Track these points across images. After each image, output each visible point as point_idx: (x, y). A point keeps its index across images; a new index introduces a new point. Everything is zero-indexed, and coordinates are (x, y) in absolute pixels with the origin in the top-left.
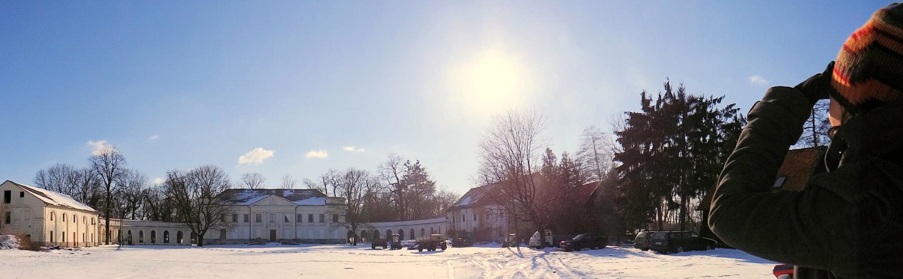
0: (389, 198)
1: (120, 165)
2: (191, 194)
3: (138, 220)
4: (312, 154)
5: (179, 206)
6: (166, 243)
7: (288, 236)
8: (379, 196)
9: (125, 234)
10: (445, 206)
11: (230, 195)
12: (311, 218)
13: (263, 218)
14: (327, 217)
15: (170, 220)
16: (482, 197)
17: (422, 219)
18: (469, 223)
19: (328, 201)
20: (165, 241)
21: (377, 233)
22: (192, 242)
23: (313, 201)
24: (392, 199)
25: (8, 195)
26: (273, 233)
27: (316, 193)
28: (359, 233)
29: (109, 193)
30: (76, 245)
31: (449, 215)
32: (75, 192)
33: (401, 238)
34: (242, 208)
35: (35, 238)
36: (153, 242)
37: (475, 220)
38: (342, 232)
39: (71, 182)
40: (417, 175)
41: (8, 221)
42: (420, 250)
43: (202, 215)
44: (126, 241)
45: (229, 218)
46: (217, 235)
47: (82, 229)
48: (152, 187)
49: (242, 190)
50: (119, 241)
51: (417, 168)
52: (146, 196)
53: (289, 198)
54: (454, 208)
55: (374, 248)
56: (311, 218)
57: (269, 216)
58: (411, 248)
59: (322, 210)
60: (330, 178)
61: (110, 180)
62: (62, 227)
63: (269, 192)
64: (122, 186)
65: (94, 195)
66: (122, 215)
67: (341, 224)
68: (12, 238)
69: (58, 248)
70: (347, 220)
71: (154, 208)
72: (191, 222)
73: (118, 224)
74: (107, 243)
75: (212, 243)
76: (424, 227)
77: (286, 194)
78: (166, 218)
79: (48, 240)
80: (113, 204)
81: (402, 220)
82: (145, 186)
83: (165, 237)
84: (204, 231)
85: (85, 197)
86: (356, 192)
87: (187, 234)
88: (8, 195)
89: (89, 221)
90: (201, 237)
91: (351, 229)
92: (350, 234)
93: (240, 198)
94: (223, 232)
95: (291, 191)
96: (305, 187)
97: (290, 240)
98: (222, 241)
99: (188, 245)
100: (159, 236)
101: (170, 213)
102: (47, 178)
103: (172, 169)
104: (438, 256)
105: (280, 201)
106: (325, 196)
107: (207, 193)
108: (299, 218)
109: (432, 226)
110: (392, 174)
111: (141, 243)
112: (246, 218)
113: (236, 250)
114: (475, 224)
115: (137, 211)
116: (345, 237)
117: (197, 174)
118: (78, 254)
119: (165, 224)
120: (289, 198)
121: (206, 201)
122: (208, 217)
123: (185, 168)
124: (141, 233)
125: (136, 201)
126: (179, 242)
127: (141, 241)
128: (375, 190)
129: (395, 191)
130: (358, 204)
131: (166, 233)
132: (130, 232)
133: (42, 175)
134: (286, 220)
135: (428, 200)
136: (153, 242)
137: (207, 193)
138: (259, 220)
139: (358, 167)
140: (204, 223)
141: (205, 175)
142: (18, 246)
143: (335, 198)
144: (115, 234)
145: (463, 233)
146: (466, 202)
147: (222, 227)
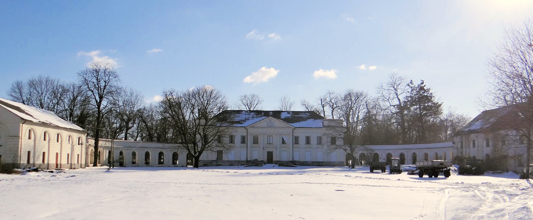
0: (390, 120)
1: (113, 82)
2: (188, 115)
3: (132, 141)
4: (319, 73)
5: (174, 127)
6: (161, 164)
7: (285, 157)
8: (380, 118)
9: (116, 156)
10: (454, 129)
11: (226, 116)
12: (308, 140)
14: (324, 139)
15: (166, 141)
16: (493, 122)
17: (426, 142)
18: (480, 149)
19: (326, 123)
20: (160, 163)
21: (376, 156)
22: (188, 164)
23: (310, 122)
24: (393, 121)
26: (270, 155)
27: (314, 115)
28: (357, 155)
29: (99, 112)
30: (59, 168)
31: (457, 139)
32: (60, 108)
33: (402, 161)
34: (239, 130)
36: (147, 164)
37: (488, 145)
38: (339, 155)
39: (56, 97)
40: (422, 98)
42: (421, 176)
43: (198, 136)
44: (117, 162)
45: (226, 140)
46: (213, 156)
47: (67, 150)
48: (147, 106)
49: (239, 112)
51: (422, 88)
52: (141, 116)
53: (286, 120)
54: (462, 132)
55: (372, 171)
56: (308, 140)
57: (266, 137)
58: (412, 173)
59: (320, 133)
60: (328, 99)
61: (101, 98)
62: (43, 147)
63: (266, 114)
64: (115, 104)
65: (82, 114)
66: (114, 135)
67: (340, 147)
69: (36, 170)
70: (345, 144)
71: (149, 129)
72: (186, 143)
73: (109, 144)
74: (95, 165)
75: (208, 165)
76: (426, 151)
77: (283, 116)
78: (161, 138)
80: (104, 123)
81: (403, 144)
83: (160, 158)
84: (200, 153)
85: (71, 115)
86: (354, 114)
89: (76, 141)
90: (197, 158)
91: (349, 152)
92: (349, 156)
93: (237, 119)
94: (220, 153)
95: (289, 112)
96: (302, 109)
97: (287, 162)
98: (218, 163)
99: (184, 167)
100: (154, 157)
101: (166, 133)
102: (26, 90)
103: (168, 89)
104: (440, 182)
105: (277, 122)
106: (321, 118)
107: (203, 114)
108: (296, 140)
109: (437, 150)
110: (393, 95)
111: (134, 165)
112: (244, 140)
113: (232, 171)
114: (488, 150)
115: (130, 131)
116: (343, 159)
117: (194, 95)
118: (61, 176)
119: (160, 145)
120: (286, 120)
121: (203, 122)
122: (205, 138)
123: (181, 88)
124: (134, 154)
125: (129, 120)
126: (174, 163)
127: (134, 163)
128: (375, 112)
129: (396, 113)
130: (357, 125)
131: (161, 154)
132: (121, 153)
133: (19, 87)
134: (283, 142)
135: (434, 124)
136: (147, 163)
137: (203, 114)
138: (256, 141)
139: (356, 89)
140: (200, 145)
143: (333, 120)
144: (105, 155)
145: (473, 161)
146: (477, 126)
147: (218, 149)
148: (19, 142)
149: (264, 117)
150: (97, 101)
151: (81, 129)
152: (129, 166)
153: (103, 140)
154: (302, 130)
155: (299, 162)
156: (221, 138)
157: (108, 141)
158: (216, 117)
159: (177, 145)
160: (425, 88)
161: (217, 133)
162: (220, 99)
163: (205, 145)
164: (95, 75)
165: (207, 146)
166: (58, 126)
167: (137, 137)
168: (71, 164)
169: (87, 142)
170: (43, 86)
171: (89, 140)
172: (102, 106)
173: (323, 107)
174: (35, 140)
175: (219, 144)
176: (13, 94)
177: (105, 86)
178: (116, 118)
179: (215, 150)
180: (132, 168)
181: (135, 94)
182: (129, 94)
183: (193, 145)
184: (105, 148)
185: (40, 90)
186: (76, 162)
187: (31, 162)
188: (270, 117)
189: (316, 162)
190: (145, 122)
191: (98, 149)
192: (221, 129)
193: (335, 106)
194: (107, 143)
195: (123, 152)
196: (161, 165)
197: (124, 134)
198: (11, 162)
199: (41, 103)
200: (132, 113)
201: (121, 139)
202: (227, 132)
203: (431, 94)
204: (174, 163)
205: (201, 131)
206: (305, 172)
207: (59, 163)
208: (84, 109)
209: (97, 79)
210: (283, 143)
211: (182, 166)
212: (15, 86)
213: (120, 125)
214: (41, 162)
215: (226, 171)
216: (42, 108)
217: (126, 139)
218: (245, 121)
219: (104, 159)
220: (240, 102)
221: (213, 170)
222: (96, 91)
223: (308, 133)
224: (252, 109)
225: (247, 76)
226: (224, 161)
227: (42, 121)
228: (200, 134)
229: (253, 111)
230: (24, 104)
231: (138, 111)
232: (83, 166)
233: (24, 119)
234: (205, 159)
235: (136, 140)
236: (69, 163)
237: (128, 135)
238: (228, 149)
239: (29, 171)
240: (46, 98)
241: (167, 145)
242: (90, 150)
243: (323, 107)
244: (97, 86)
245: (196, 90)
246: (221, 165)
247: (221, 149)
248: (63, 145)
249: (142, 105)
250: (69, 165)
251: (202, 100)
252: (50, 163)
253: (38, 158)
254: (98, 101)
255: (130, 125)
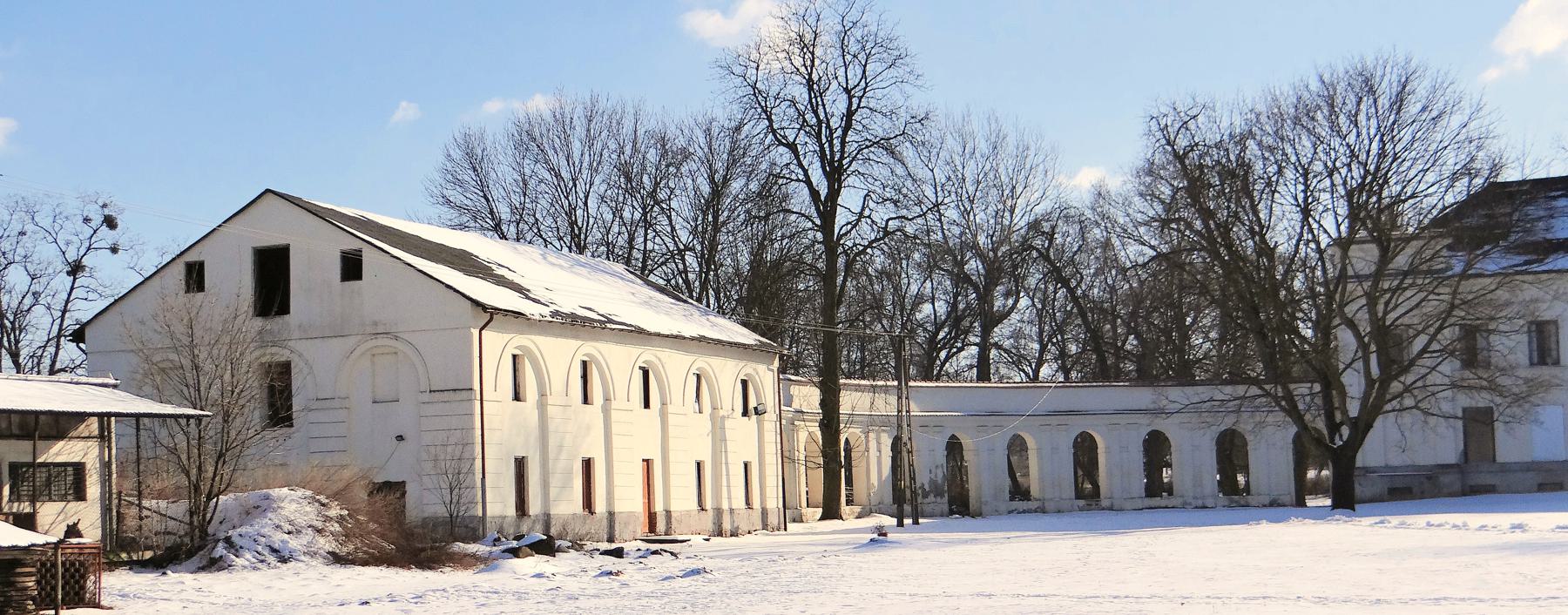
1: (1207, 132)
3: (1015, 393)
6: (1158, 495)
9: (928, 463)
15: (1184, 374)
25: (272, 269)
30: (141, 519)
35: (425, 502)
36: (1086, 496)
39: (630, 191)
41: (279, 411)
44: (939, 494)
45: (1510, 346)
46: (1442, 444)
50: (898, 497)
52: (1029, 254)
68: (293, 504)
69: (546, 547)
75: (1412, 489)
78: (1164, 364)
79: (499, 504)
82: (1032, 204)
84: (1361, 427)
87: (1271, 452)
88: (272, 269)
89: (731, 398)
94: (1478, 424)
99: (1197, 510)
100: (1119, 463)
102: (503, 173)
107: (1371, 213)
111: (1021, 500)
115: (1001, 333)
117: (1303, 116)
119: (1143, 396)
121: (1364, 257)
122: (1387, 345)
123: (1230, 91)
124: (1017, 446)
127: (1019, 492)
132: (954, 447)
137: (1371, 213)
140: (1353, 383)
141: (1367, 109)
142: (326, 544)
144: (873, 466)
147: (1465, 400)
148: (472, 415)
150: (814, 194)
151: (750, 338)
152: (997, 513)
153: (858, 388)
156: (1481, 342)
157: (886, 389)
158: (1447, 221)
159: (1240, 390)
161: (1449, 313)
162: (1456, 121)
163: (1385, 381)
164: (798, 62)
165: (1396, 387)
166: (640, 331)
167: (1040, 363)
168: (718, 512)
169: (785, 399)
170: (576, 147)
171: (795, 390)
172: (841, 218)
174: (542, 405)
175: (1467, 374)
176: (455, 195)
177: (849, 115)
178: (929, 269)
179: (1446, 407)
180: (1147, 515)
181: (1011, 142)
182: (983, 147)
183: (1317, 387)
184: (872, 423)
185: (563, 163)
186: (739, 502)
190: (1065, 283)
191: (837, 432)
192: (1470, 287)
194: (880, 399)
195: (966, 442)
196: (1017, 504)
197: (974, 350)
198: (441, 511)
199: (573, 224)
200: (1005, 239)
201: (957, 375)
202: (1508, 304)
204: (1228, 486)
205: (1356, 309)
207: (659, 507)
208: (767, 238)
209: (810, 83)
211: (1274, 504)
212: (457, 154)
213: (953, 306)
214: (577, 505)
216: (581, 249)
217: (984, 375)
219: (874, 480)
221: (1410, 519)
222: (808, 145)
226: (1506, 468)
227: (566, 310)
228: (1351, 324)
230: (503, 237)
231: (1034, 226)
232: (773, 520)
233: (483, 307)
234: (1396, 460)
235: (1036, 378)
236: (709, 504)
237: (993, 353)
238: (1518, 399)
239: (515, 553)
240: (592, 203)
241: (1177, 395)
242: (803, 436)
244: (809, 117)
245: (1315, 86)
246: (1490, 489)
247: (1482, 400)
248: (671, 419)
249: (1051, 193)
250: (709, 516)
251: (1352, 139)
252: (619, 508)
253: (566, 485)
254: (823, 192)
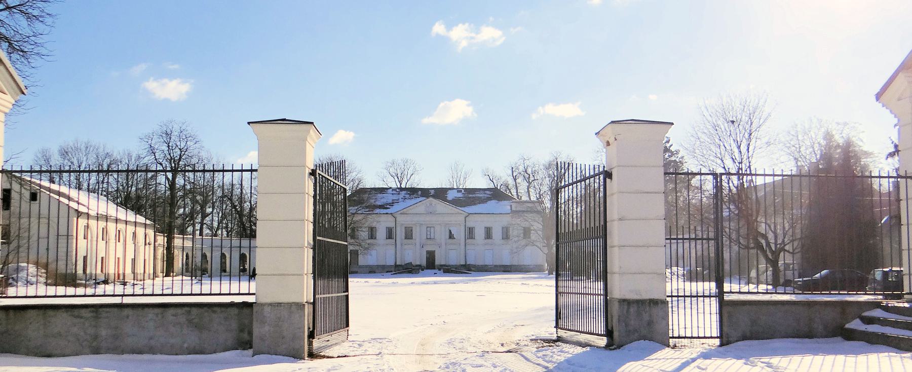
7: (455, 259)
12: (488, 234)
13: (416, 233)
23: (492, 205)
26: (431, 256)
27: (496, 194)
34: (383, 218)
49: (382, 190)
53: (456, 202)
56: (488, 234)
59: (506, 220)
60: (521, 168)
63: (425, 193)
77: (451, 196)
95: (459, 190)
106: (509, 198)
112: (390, 234)
113: (372, 281)
134: (451, 236)
138: (409, 235)
149: (421, 199)
154: (482, 217)
155: (474, 266)
156: (357, 233)
160: (672, 149)
173: (515, 180)
186: (99, 271)
187: (88, 272)
188: (431, 199)
189: (501, 266)
193: (532, 179)
203: (682, 157)
206: (476, 280)
207: (121, 272)
210: (450, 237)
212: (40, 156)
215: (363, 280)
218: (392, 204)
220: (385, 172)
223: (487, 221)
224: (403, 186)
225: (433, 24)
226: (361, 267)
229: (406, 189)
237: (205, 226)
238: (367, 249)
243: (515, 180)
246: (356, 272)
247: (357, 248)
255: (209, 210)
